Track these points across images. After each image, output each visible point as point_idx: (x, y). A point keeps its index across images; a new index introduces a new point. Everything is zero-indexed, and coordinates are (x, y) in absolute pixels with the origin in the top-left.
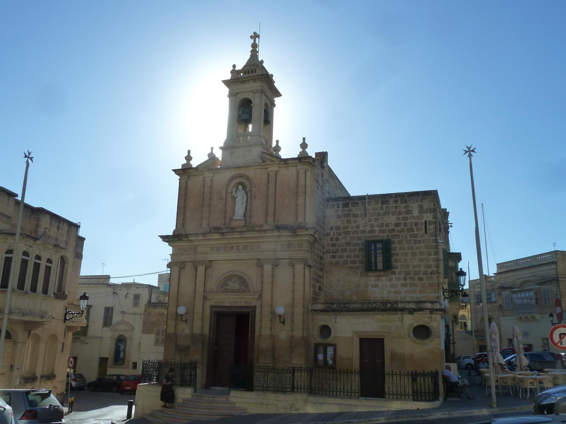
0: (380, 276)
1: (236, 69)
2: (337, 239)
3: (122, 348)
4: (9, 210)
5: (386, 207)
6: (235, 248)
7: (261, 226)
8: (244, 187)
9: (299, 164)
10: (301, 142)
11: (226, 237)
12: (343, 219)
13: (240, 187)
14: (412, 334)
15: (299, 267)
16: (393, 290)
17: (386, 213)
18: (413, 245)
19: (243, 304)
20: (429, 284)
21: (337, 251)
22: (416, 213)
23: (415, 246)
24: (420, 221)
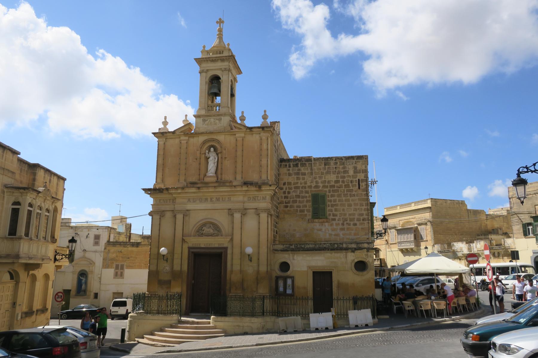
0: (324, 222)
1: (206, 49)
2: (289, 193)
3: (83, 281)
4: (14, 166)
5: (328, 168)
6: (209, 200)
7: (231, 182)
8: (215, 150)
9: (262, 132)
10: (263, 113)
11: (202, 191)
12: (293, 176)
13: (212, 149)
14: (353, 268)
15: (264, 216)
16: (333, 233)
17: (328, 173)
18: (349, 198)
19: (217, 246)
20: (362, 228)
21: (289, 202)
22: (351, 172)
23: (351, 199)
24: (354, 179)
